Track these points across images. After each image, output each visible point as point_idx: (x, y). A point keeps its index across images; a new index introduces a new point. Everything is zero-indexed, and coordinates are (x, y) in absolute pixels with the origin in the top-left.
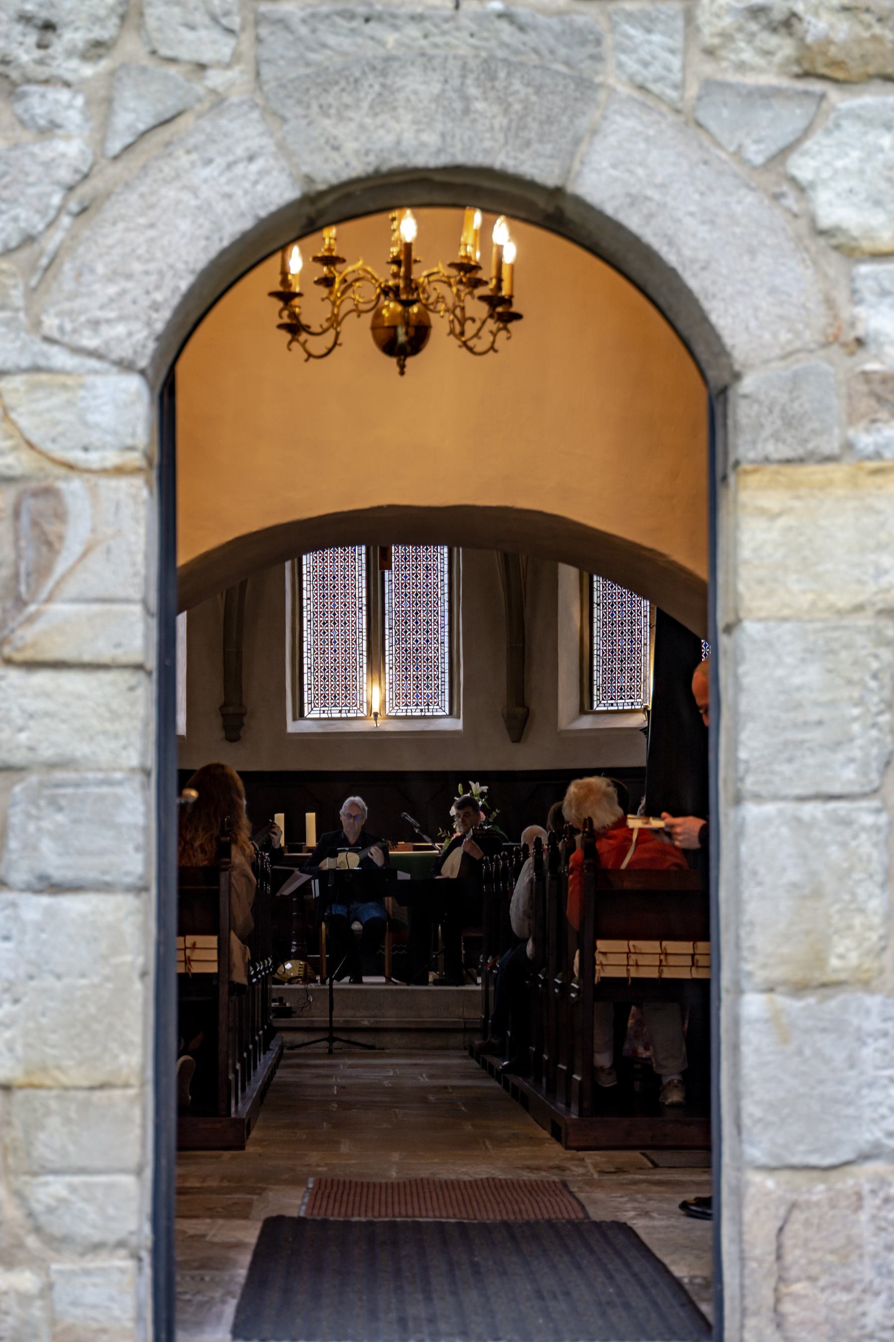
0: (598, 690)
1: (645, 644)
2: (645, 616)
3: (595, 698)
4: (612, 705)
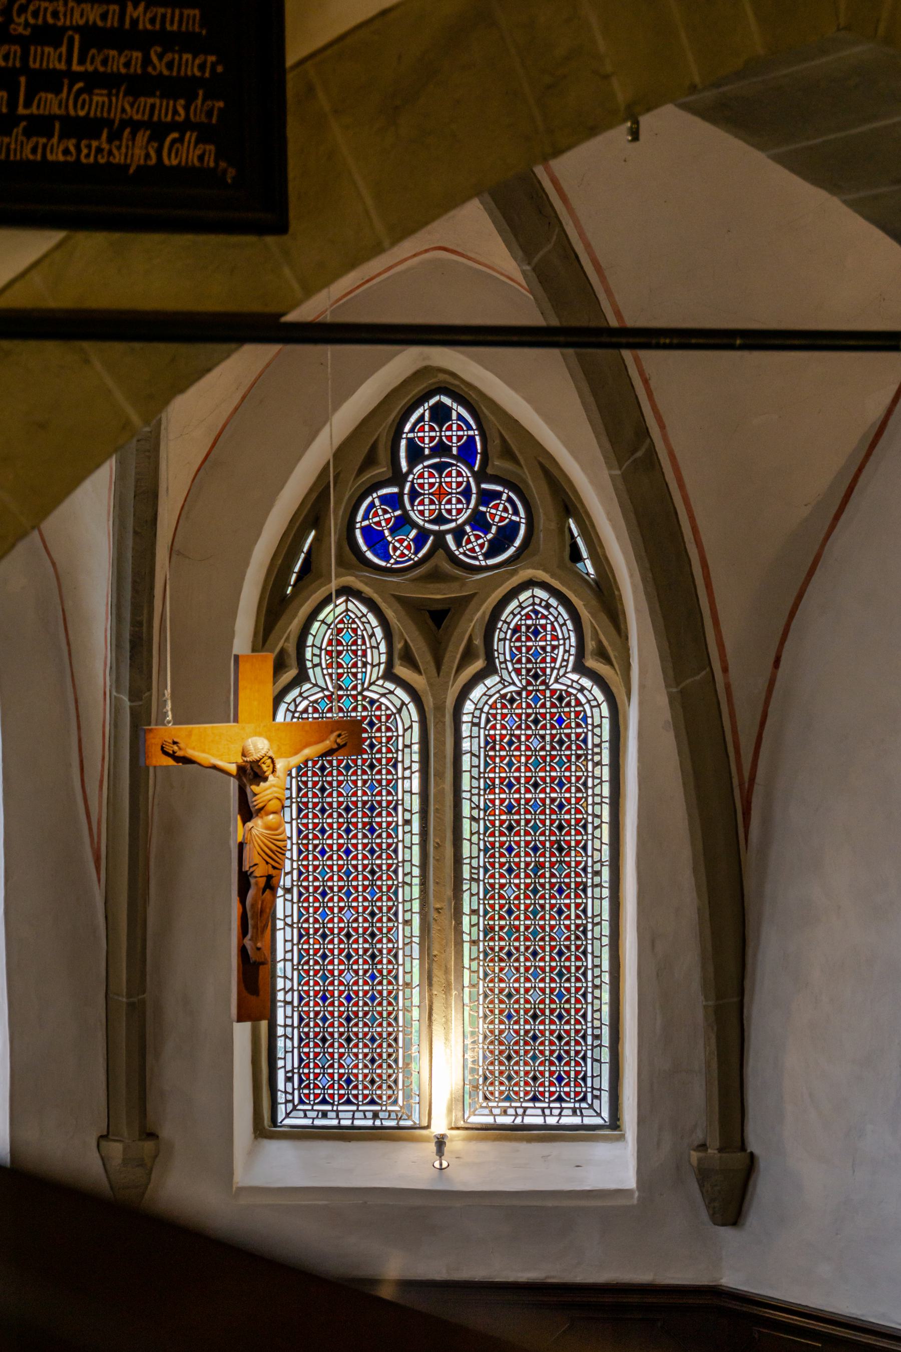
0: (289, 1079)
1: (407, 985)
2: (407, 922)
3: (281, 1098)
4: (325, 1115)
